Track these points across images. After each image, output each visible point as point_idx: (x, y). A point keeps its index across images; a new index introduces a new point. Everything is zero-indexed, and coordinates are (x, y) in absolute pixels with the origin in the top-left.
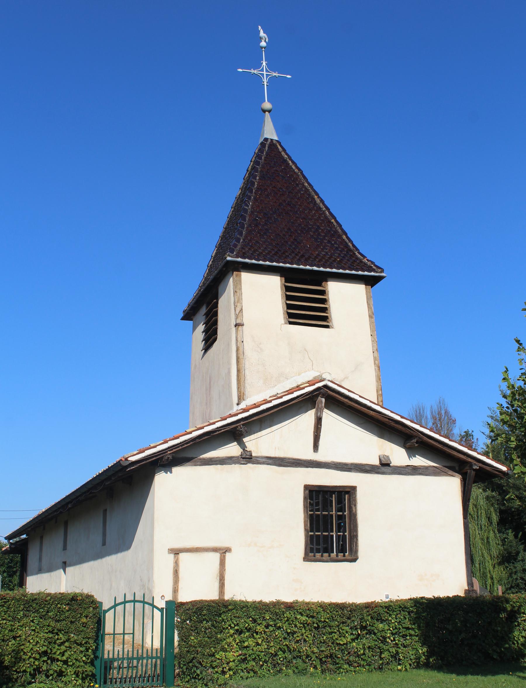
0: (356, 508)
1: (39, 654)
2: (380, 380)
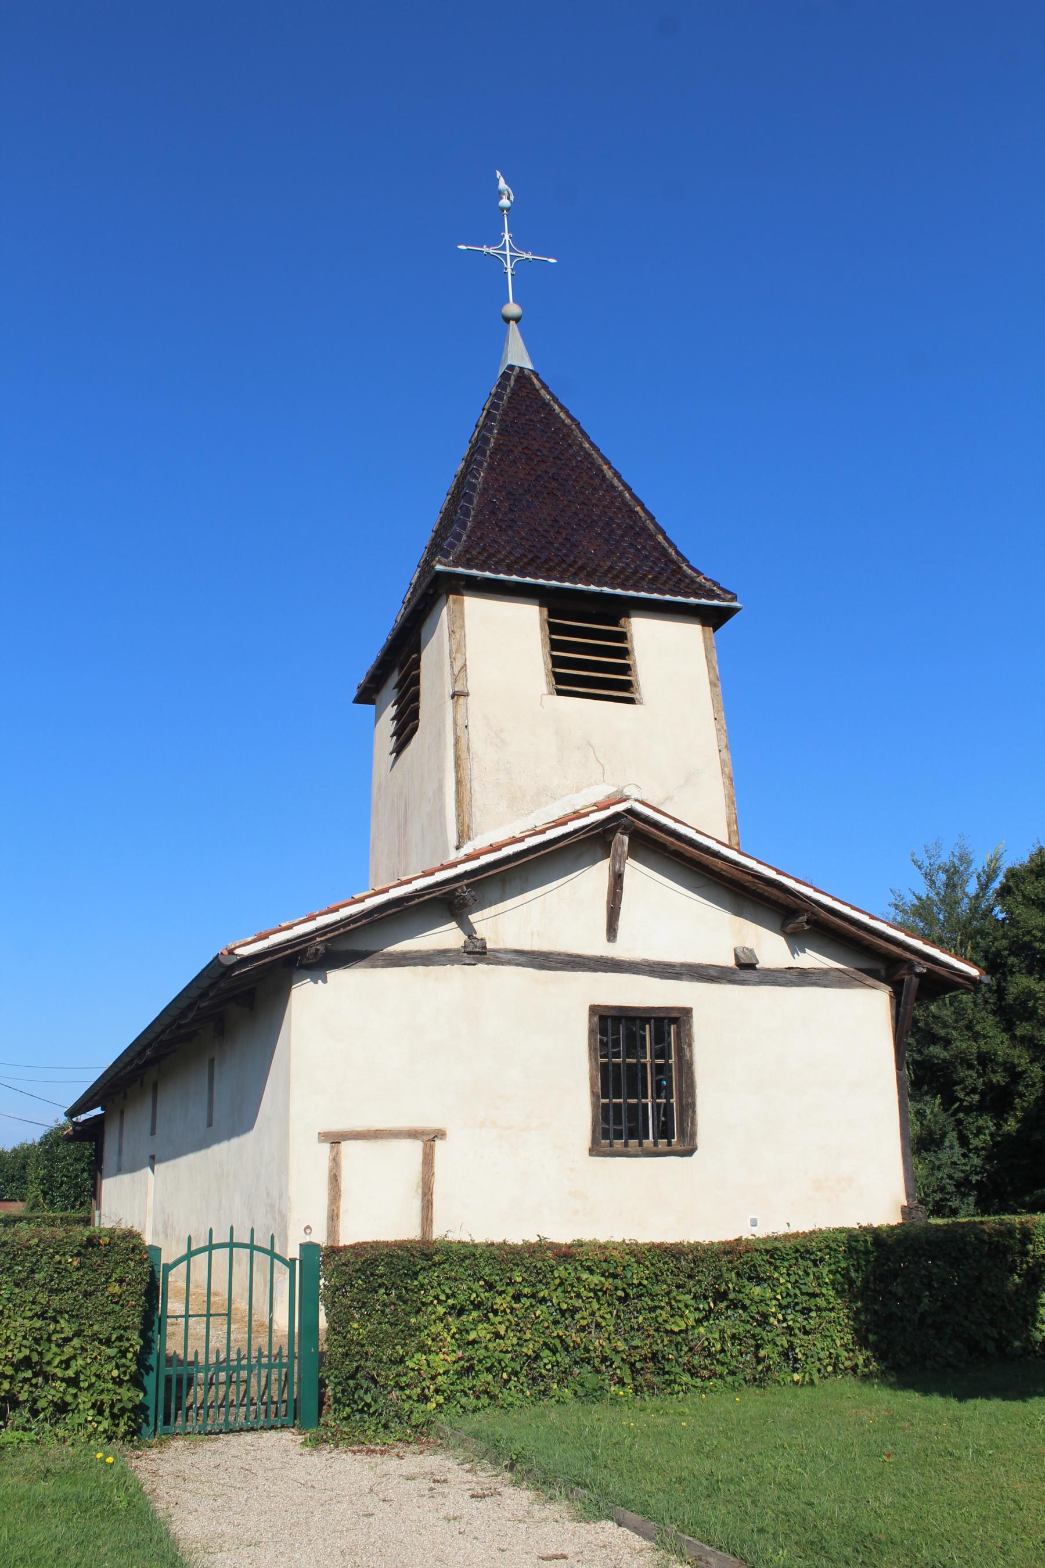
0: (691, 1051)
1: (12, 1364)
2: (733, 803)
